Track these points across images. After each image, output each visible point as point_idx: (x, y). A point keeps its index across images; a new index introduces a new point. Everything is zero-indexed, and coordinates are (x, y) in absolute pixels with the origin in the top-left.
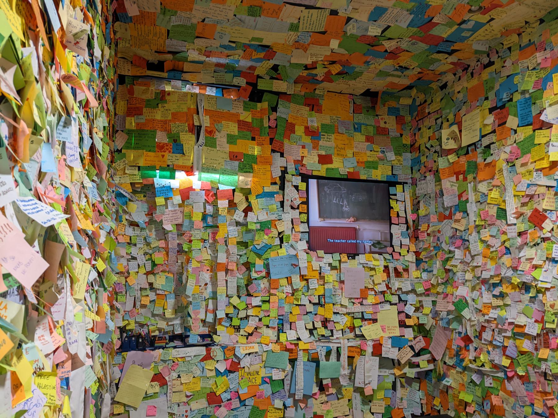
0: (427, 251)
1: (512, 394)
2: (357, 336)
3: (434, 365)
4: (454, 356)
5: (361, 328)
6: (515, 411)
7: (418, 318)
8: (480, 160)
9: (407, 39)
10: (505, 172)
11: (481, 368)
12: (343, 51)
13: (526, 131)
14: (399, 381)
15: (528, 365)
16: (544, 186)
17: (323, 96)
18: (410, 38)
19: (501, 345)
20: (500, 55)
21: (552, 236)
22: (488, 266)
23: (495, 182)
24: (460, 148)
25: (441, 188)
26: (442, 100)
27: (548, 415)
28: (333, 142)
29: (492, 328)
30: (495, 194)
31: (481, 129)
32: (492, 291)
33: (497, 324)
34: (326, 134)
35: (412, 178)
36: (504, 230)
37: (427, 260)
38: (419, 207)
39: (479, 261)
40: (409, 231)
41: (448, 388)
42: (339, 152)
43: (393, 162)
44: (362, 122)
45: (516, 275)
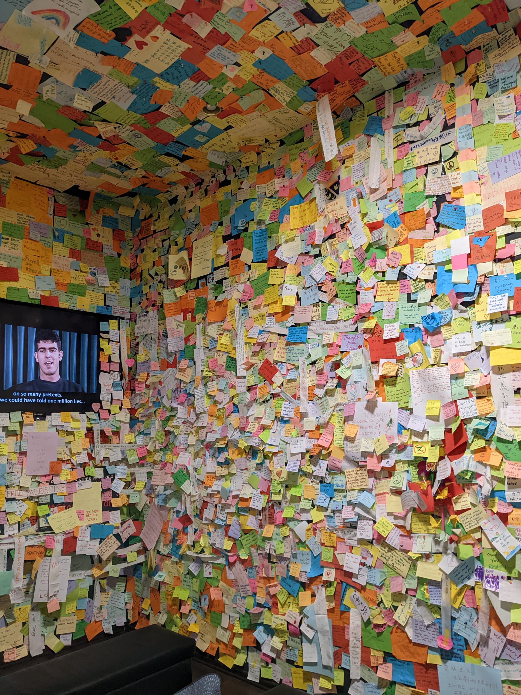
0: (145, 407)
1: (232, 583)
2: (40, 530)
3: (146, 556)
4: (170, 542)
5: (48, 518)
6: (236, 604)
7: (128, 496)
8: (210, 297)
9: (128, 127)
10: (237, 314)
11: (200, 555)
12: (37, 122)
13: (260, 268)
14: (98, 583)
15: (252, 546)
16: (276, 333)
17: (7, 182)
18: (131, 125)
19: (224, 523)
20: (237, 173)
21: (282, 391)
22: (214, 427)
23: (226, 325)
24: (190, 280)
25: (165, 328)
26: (170, 217)
27: (270, 605)
28: (20, 251)
29: (215, 503)
30: (225, 340)
31: (213, 260)
32: (217, 458)
33: (221, 498)
34: (10, 238)
35: (130, 312)
36: (233, 383)
37: (144, 419)
38: (138, 350)
39: (205, 420)
40: (123, 381)
41: (160, 584)
42: (28, 266)
43: (106, 289)
44: (66, 229)
45: (244, 438)
